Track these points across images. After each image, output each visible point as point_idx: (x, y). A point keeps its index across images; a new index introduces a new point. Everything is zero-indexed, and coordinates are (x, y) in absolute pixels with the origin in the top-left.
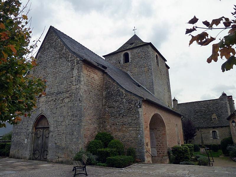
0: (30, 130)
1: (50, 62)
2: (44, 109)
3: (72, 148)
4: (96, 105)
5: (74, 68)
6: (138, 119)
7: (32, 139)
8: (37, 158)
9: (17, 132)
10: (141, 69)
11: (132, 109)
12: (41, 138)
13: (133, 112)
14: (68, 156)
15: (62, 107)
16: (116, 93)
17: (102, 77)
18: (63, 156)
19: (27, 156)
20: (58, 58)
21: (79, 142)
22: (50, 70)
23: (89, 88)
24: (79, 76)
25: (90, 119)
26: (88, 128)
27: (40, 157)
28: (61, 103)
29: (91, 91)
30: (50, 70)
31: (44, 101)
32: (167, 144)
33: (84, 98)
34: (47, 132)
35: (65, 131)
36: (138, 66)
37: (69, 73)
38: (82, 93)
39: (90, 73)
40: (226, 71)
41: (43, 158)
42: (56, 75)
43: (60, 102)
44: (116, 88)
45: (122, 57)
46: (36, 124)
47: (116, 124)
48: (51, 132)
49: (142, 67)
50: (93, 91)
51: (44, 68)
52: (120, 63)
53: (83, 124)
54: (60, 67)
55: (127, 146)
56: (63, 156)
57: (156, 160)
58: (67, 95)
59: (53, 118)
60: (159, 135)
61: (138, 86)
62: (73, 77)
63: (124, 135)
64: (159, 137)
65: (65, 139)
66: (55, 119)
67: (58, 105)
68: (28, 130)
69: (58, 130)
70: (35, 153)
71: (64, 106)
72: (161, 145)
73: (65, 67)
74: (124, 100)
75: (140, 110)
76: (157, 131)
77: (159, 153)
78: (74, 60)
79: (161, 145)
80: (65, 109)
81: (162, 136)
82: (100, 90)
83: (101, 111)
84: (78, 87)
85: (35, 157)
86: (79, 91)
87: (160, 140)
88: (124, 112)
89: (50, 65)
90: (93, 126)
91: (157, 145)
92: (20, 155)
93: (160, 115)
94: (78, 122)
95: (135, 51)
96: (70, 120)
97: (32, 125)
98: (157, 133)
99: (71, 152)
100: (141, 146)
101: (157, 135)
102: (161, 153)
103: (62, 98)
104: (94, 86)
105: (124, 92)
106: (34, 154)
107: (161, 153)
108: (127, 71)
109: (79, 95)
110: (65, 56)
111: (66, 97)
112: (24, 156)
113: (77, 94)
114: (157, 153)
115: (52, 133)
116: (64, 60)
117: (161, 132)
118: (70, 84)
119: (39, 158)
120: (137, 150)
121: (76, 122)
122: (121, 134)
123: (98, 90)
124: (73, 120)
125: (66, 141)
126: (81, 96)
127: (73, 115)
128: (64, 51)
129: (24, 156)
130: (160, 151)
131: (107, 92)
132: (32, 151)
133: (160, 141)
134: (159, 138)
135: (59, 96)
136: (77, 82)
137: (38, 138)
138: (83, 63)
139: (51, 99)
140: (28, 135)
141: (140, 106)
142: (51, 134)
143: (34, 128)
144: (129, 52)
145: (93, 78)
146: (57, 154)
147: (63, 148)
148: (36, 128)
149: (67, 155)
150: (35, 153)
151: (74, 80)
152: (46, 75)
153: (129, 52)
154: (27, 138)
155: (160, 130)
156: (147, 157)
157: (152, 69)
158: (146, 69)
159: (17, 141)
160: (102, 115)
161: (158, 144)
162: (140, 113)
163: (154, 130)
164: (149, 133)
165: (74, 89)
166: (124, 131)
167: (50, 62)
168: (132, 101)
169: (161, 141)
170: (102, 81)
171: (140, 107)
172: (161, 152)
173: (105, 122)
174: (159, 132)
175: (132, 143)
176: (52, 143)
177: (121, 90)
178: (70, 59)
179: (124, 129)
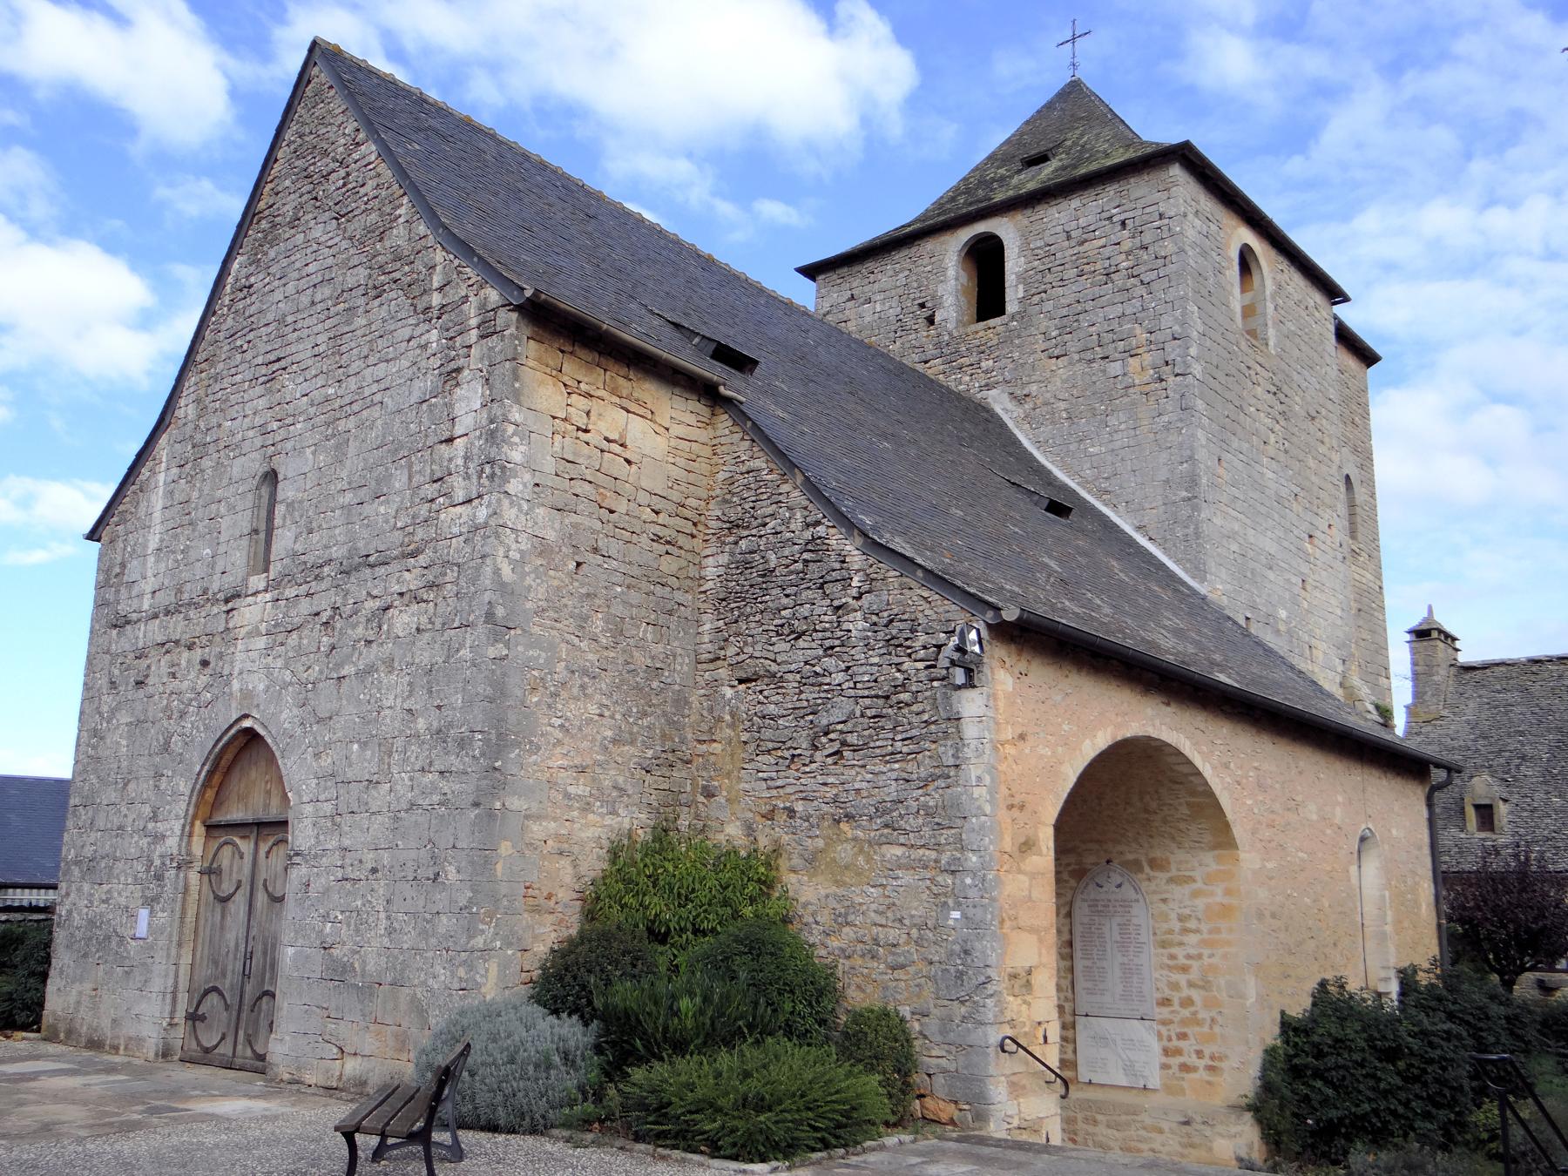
0: (172, 844)
1: (308, 322)
2: (261, 687)
3: (424, 983)
4: (641, 660)
5: (458, 370)
6: (947, 773)
7: (179, 905)
8: (207, 1051)
9: (88, 851)
10: (1104, 371)
11: (905, 697)
12: (240, 900)
13: (915, 719)
15: (370, 670)
16: (799, 566)
17: (703, 435)
18: (369, 1043)
20: (361, 290)
21: (479, 942)
22: (306, 387)
23: (575, 526)
25: (582, 770)
26: (558, 837)
27: (229, 1040)
28: (369, 642)
29: (596, 550)
30: (306, 387)
31: (263, 628)
32: (1242, 996)
33: (529, 605)
34: (278, 859)
35: (386, 857)
36: (1073, 347)
37: (424, 406)
38: (517, 565)
39: (594, 405)
41: (249, 1053)
43: (360, 630)
44: (796, 525)
45: (951, 273)
46: (210, 794)
47: (791, 812)
49: (1109, 350)
50: (614, 547)
51: (264, 370)
52: (931, 320)
53: (515, 803)
54: (371, 360)
55: (859, 987)
56: (369, 1043)
57: (1148, 1121)
58: (412, 580)
59: (317, 756)
60: (1181, 918)
61: (1048, 509)
62: (450, 440)
64: (1185, 931)
65: (382, 915)
66: (326, 761)
68: (159, 838)
69: (347, 842)
70: (200, 1013)
71: (389, 663)
72: (1196, 995)
73: (405, 363)
74: (856, 625)
75: (970, 704)
76: (1171, 880)
77: (1175, 1061)
78: (465, 307)
79: (1196, 995)
80: (393, 691)
81: (1204, 927)
82: (682, 540)
83: (681, 702)
84: (482, 514)
85: (199, 1044)
86: (487, 549)
87: (1189, 957)
88: (851, 715)
89: (303, 352)
90: (608, 820)
91: (1165, 1002)
92: (106, 1023)
93: (1179, 753)
94: (470, 788)
95: (1059, 216)
96: (423, 770)
97: (184, 806)
98: (1164, 901)
99: (420, 1011)
101: (1166, 918)
102: (1194, 1069)
103: (377, 603)
104: (622, 507)
105: (856, 559)
107: (1194, 1069)
108: (988, 387)
109: (487, 579)
110: (403, 272)
111: (401, 594)
112: (132, 1033)
113: (478, 569)
114: (1165, 1067)
115: (304, 870)
116: (400, 308)
117: (1196, 894)
118: (430, 490)
120: (932, 1026)
121: (457, 787)
122: (823, 892)
123: (657, 539)
125: (390, 931)
126: (501, 586)
127: (439, 734)
128: (398, 236)
129: (129, 1029)
130: (1182, 1044)
131: (732, 554)
132: (183, 998)
133: (1185, 969)
134: (1181, 944)
136: (480, 477)
137: (224, 900)
138: (527, 331)
139: (305, 607)
140: (159, 877)
141: (969, 672)
142: (298, 874)
143: (198, 823)
144: (1004, 228)
145: (616, 448)
147: (368, 990)
148: (211, 828)
149: (396, 1036)
150: (200, 1013)
151: (460, 462)
152: (275, 425)
153: (1004, 228)
154: (150, 902)
155: (1192, 879)
156: (1016, 1089)
157: (1197, 369)
158: (1139, 370)
159: (91, 923)
160: (690, 736)
161: (1175, 986)
162: (970, 731)
163: (1147, 869)
164: (1045, 894)
165: (455, 530)
166: (847, 867)
167: (308, 322)
168: (913, 631)
169: (1195, 964)
170: (701, 466)
171: (970, 684)
172: (1193, 1060)
173: (709, 794)
174: (1187, 889)
175: (902, 967)
176: (300, 942)
177: (837, 539)
179: (844, 852)
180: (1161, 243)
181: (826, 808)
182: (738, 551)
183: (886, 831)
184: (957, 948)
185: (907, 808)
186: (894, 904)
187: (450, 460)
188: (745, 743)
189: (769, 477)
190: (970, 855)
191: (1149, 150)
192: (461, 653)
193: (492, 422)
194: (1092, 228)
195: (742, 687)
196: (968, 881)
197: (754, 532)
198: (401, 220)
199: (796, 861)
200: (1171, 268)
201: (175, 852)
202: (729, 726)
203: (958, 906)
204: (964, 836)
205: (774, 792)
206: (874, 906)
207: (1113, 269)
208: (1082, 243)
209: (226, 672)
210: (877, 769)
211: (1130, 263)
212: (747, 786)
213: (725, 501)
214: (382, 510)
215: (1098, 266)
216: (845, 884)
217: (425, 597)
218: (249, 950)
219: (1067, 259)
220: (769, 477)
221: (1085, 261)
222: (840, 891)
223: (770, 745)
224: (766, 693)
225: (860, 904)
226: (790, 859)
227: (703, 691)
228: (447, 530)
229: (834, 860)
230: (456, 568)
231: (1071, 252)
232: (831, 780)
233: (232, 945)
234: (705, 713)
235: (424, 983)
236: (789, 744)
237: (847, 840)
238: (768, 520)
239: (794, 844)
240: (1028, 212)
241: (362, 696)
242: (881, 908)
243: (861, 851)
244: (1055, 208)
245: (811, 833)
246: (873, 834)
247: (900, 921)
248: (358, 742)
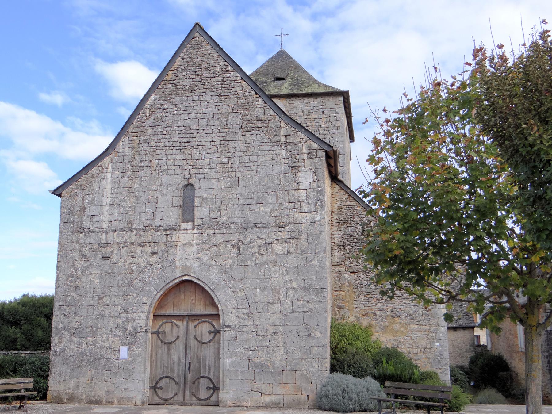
2: (196, 265)
5: (299, 167)
14: (298, 389)
15: (263, 264)
19: (132, 395)
22: (208, 156)
24: (320, 191)
31: (194, 243)
35: (281, 329)
40: (368, 163)
42: (233, 174)
47: (375, 314)
48: (228, 329)
54: (248, 153)
63: (395, 340)
67: (250, 259)
69: (257, 323)
97: (147, 308)
100: (440, 366)
106: (154, 388)
111: (277, 239)
119: (180, 398)
122: (388, 338)
124: (308, 301)
127: (306, 289)
135: (250, 235)
146: (257, 386)
148: (156, 316)
166: (397, 331)
175: (419, 359)
178: (283, 139)
179: (396, 327)
180: (336, 122)
181: (388, 313)
182: (347, 231)
183: (411, 321)
184: (438, 354)
185: (418, 314)
186: (415, 342)
187: (299, 197)
188: (355, 292)
189: (357, 209)
190: (441, 328)
191: (332, 90)
192: (313, 262)
193: (319, 187)
194: (312, 111)
195: (352, 274)
196: (441, 335)
197: (353, 225)
198: (259, 106)
199: (377, 329)
200: (339, 131)
201: (143, 325)
202: (347, 286)
203: (438, 342)
204: (439, 322)
205: (368, 308)
206: (408, 342)
207: (319, 127)
208: (309, 115)
209: (170, 257)
210: (407, 302)
211: (326, 126)
212: (356, 306)
213: (339, 214)
214: (262, 208)
215: (314, 124)
216: (397, 336)
217: (291, 242)
218: (188, 361)
219: (303, 120)
220: (357, 209)
221: (309, 122)
222: (395, 338)
223: (365, 293)
224: (362, 277)
225: (402, 342)
226: (376, 329)
227: (335, 275)
228: (300, 221)
229: (392, 329)
230: (306, 234)
231: (304, 117)
232: (389, 305)
233: (176, 360)
234: (337, 282)
235: (308, 369)
236: (373, 293)
237: (397, 323)
238: (358, 222)
239: (376, 324)
240: (288, 100)
241: (260, 273)
242: (410, 343)
243: (403, 326)
244: (298, 101)
245: (383, 321)
246: (406, 321)
247: (418, 346)
248: (260, 288)
